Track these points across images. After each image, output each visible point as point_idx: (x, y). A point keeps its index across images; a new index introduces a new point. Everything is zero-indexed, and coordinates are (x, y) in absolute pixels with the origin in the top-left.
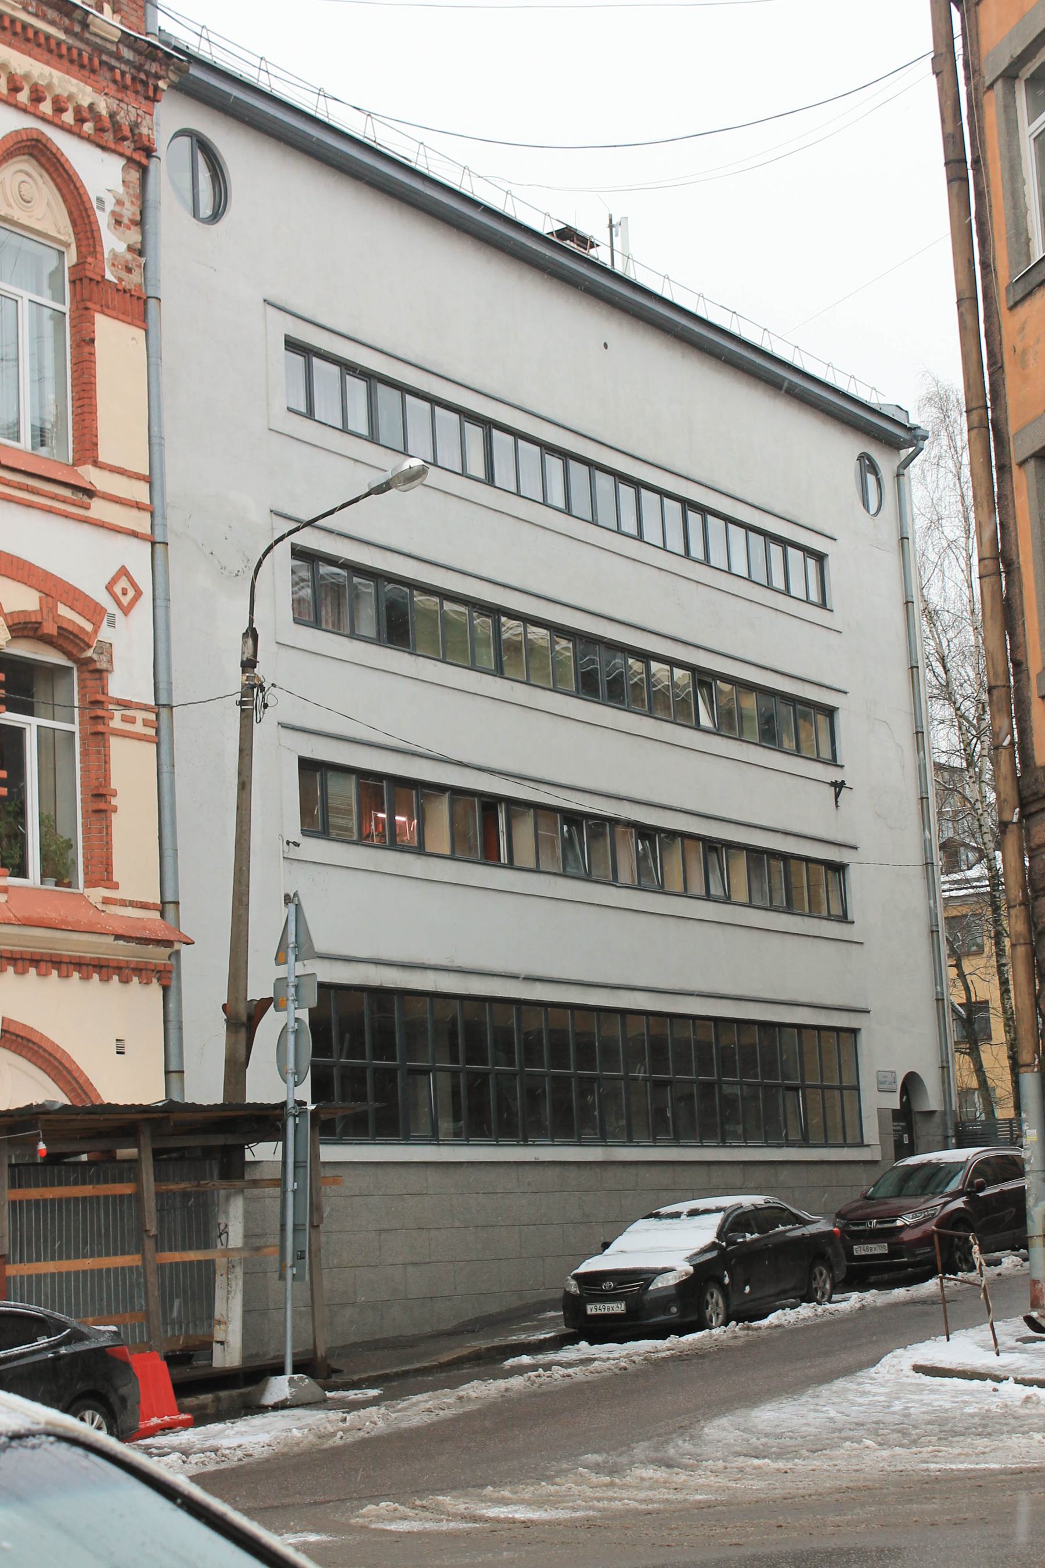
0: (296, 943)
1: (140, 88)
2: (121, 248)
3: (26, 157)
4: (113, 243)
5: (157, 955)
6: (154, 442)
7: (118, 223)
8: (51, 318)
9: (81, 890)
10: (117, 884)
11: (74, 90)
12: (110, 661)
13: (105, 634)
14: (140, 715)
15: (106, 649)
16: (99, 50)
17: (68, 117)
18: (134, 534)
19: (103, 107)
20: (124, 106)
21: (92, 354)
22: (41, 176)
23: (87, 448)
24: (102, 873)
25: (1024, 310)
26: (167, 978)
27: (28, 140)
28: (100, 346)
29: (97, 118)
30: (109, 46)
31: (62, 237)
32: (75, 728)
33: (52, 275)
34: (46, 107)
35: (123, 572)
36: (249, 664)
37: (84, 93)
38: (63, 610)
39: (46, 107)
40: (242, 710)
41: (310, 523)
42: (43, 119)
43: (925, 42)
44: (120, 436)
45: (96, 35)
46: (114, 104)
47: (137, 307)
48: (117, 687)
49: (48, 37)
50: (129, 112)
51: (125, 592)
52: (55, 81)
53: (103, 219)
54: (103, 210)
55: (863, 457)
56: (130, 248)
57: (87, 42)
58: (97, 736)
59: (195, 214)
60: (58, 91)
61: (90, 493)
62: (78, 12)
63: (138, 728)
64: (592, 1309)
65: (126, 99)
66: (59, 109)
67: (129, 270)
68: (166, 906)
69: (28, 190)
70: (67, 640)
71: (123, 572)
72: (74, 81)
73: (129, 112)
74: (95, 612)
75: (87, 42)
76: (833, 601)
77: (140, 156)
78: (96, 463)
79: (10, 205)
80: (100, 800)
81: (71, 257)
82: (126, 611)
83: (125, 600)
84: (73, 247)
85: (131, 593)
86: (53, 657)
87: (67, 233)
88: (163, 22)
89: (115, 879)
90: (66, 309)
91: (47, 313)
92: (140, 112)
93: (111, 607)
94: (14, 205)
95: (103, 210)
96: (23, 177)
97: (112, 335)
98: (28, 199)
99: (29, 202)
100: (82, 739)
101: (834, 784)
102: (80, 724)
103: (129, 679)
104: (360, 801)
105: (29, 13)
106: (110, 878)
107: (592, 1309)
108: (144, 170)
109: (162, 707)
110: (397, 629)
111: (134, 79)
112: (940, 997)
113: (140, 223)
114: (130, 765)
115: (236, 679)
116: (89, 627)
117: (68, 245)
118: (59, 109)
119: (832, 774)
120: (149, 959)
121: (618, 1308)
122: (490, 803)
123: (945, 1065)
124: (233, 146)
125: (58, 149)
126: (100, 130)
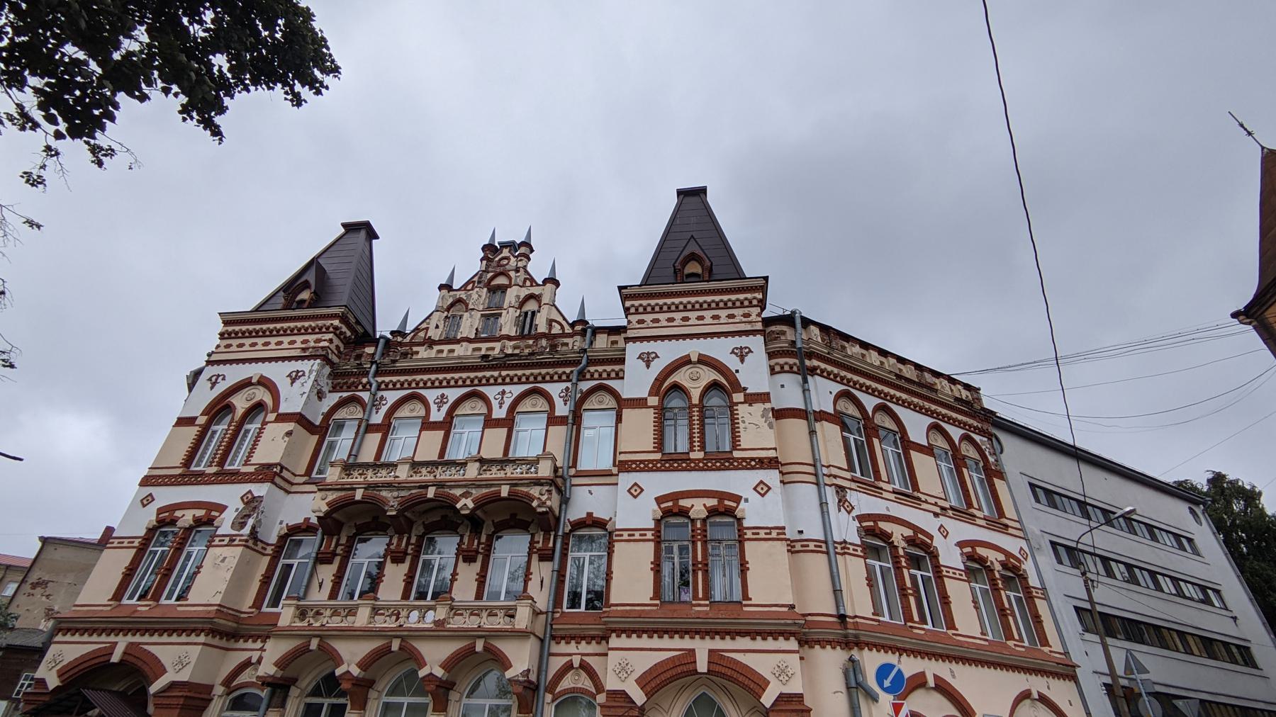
26: (1073, 678)
68: (1066, 653)
81: (981, 464)
109: (1044, 589)
124: (1002, 436)
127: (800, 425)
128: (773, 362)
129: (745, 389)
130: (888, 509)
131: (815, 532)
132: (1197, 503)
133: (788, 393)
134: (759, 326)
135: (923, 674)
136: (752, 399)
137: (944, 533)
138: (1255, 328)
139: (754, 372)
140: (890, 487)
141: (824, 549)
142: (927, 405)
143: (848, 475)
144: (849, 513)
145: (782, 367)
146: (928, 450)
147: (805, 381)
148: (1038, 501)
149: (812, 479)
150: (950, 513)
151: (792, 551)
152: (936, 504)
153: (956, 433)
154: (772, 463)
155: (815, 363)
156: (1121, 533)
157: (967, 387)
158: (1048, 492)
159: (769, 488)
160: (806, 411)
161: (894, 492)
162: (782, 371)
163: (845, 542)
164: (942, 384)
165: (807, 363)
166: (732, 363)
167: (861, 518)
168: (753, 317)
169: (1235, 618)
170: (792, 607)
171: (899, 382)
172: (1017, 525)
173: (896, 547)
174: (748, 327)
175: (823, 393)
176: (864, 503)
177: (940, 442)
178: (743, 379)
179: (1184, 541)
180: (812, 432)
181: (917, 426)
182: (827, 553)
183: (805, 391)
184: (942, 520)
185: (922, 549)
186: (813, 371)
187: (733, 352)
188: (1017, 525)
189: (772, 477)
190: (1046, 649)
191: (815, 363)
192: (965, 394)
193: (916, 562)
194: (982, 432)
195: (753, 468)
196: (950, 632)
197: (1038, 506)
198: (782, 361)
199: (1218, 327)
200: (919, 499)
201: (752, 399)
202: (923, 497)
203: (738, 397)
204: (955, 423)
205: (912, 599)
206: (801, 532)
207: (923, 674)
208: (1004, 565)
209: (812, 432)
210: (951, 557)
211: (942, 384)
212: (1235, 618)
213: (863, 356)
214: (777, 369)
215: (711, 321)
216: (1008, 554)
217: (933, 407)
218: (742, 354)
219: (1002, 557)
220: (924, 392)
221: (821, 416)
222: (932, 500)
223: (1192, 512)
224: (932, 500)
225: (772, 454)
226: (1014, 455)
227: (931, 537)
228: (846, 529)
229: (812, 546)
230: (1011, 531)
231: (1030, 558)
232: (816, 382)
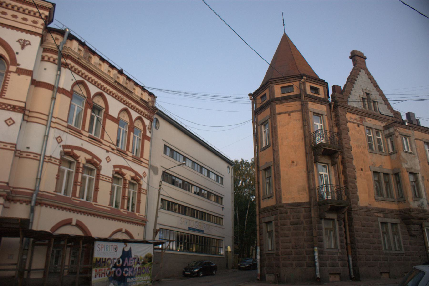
5: (144, 223)
6: (150, 156)
14: (145, 191)
15: (101, 166)
16: (149, 108)
17: (144, 115)
19: (148, 114)
23: (142, 156)
24: (138, 211)
25: (262, 152)
26: (145, 225)
34: (142, 114)
35: (145, 172)
36: (160, 186)
37: (146, 112)
39: (142, 114)
41: (168, 169)
42: (102, 90)
43: (251, 118)
44: (146, 155)
48: (143, 187)
50: (151, 115)
53: (147, 128)
55: (228, 166)
58: (140, 193)
61: (142, 162)
63: (144, 192)
64: (186, 273)
66: (144, 114)
68: (146, 216)
70: (95, 164)
71: (145, 172)
73: (151, 115)
74: (141, 177)
76: (224, 183)
77: (151, 121)
78: (143, 158)
80: (139, 202)
81: (142, 132)
82: (145, 177)
88: (156, 105)
90: (141, 138)
97: (146, 142)
104: (170, 205)
107: (186, 273)
108: (152, 122)
109: (148, 190)
110: (173, 183)
113: (151, 129)
114: (143, 197)
115: (158, 187)
118: (144, 114)
119: (222, 206)
120: (143, 223)
121: (189, 273)
122: (186, 207)
124: (161, 121)
127: (47, 93)
128: (45, 54)
129: (18, 65)
130: (82, 145)
131: (36, 148)
132: (231, 165)
133: (48, 73)
134: (40, 31)
135: (71, 219)
136: (21, 71)
137: (108, 159)
138: (252, 102)
139: (28, 58)
140: (87, 134)
141: (38, 158)
142: (125, 98)
143: (66, 124)
144: (59, 143)
145: (49, 59)
146: (117, 121)
147: (59, 70)
148: (165, 153)
149: (45, 122)
150: (115, 152)
151: (15, 156)
152: (110, 147)
153: (135, 115)
154: (22, 110)
155: (68, 61)
156: (196, 172)
157: (151, 94)
158: (172, 150)
159: (6, 121)
160: (54, 86)
161: (89, 137)
162: (49, 60)
163: (51, 157)
164: (138, 92)
165: (63, 60)
166: (16, 47)
167: (65, 147)
168: (39, 25)
169: (223, 208)
170: (8, 184)
171: (116, 86)
172: (147, 162)
173: (79, 163)
174: (33, 30)
175: (67, 79)
176: (71, 140)
177: (125, 118)
178: (19, 59)
179: (220, 178)
180: (54, 98)
181: (115, 107)
182: (39, 160)
183: (58, 76)
184: (110, 154)
185: (94, 164)
186: (66, 65)
187: (18, 41)
188: (147, 162)
189: (18, 117)
190: (137, 214)
191: (68, 61)
192: (146, 97)
193: (90, 171)
194: (148, 118)
195: (8, 110)
196: (94, 203)
197: (165, 155)
198: (50, 55)
199: (243, 98)
200: (102, 143)
201: (21, 71)
202: (104, 142)
203: (13, 68)
204: (136, 110)
205: (78, 188)
206: (28, 148)
207: (71, 219)
208: (133, 178)
209: (54, 98)
210: (107, 170)
211: (138, 92)
212: (223, 208)
213: (100, 65)
214: (46, 58)
215: (11, 18)
216: (136, 173)
217: (128, 100)
218: (24, 44)
219: (133, 174)
220: (126, 92)
221: (63, 91)
222: (108, 144)
223: (228, 167)
224: (108, 144)
225: (23, 105)
226: (165, 131)
227: (100, 161)
228: (54, 150)
229: (32, 156)
230: (143, 164)
231: (147, 177)
232: (65, 72)
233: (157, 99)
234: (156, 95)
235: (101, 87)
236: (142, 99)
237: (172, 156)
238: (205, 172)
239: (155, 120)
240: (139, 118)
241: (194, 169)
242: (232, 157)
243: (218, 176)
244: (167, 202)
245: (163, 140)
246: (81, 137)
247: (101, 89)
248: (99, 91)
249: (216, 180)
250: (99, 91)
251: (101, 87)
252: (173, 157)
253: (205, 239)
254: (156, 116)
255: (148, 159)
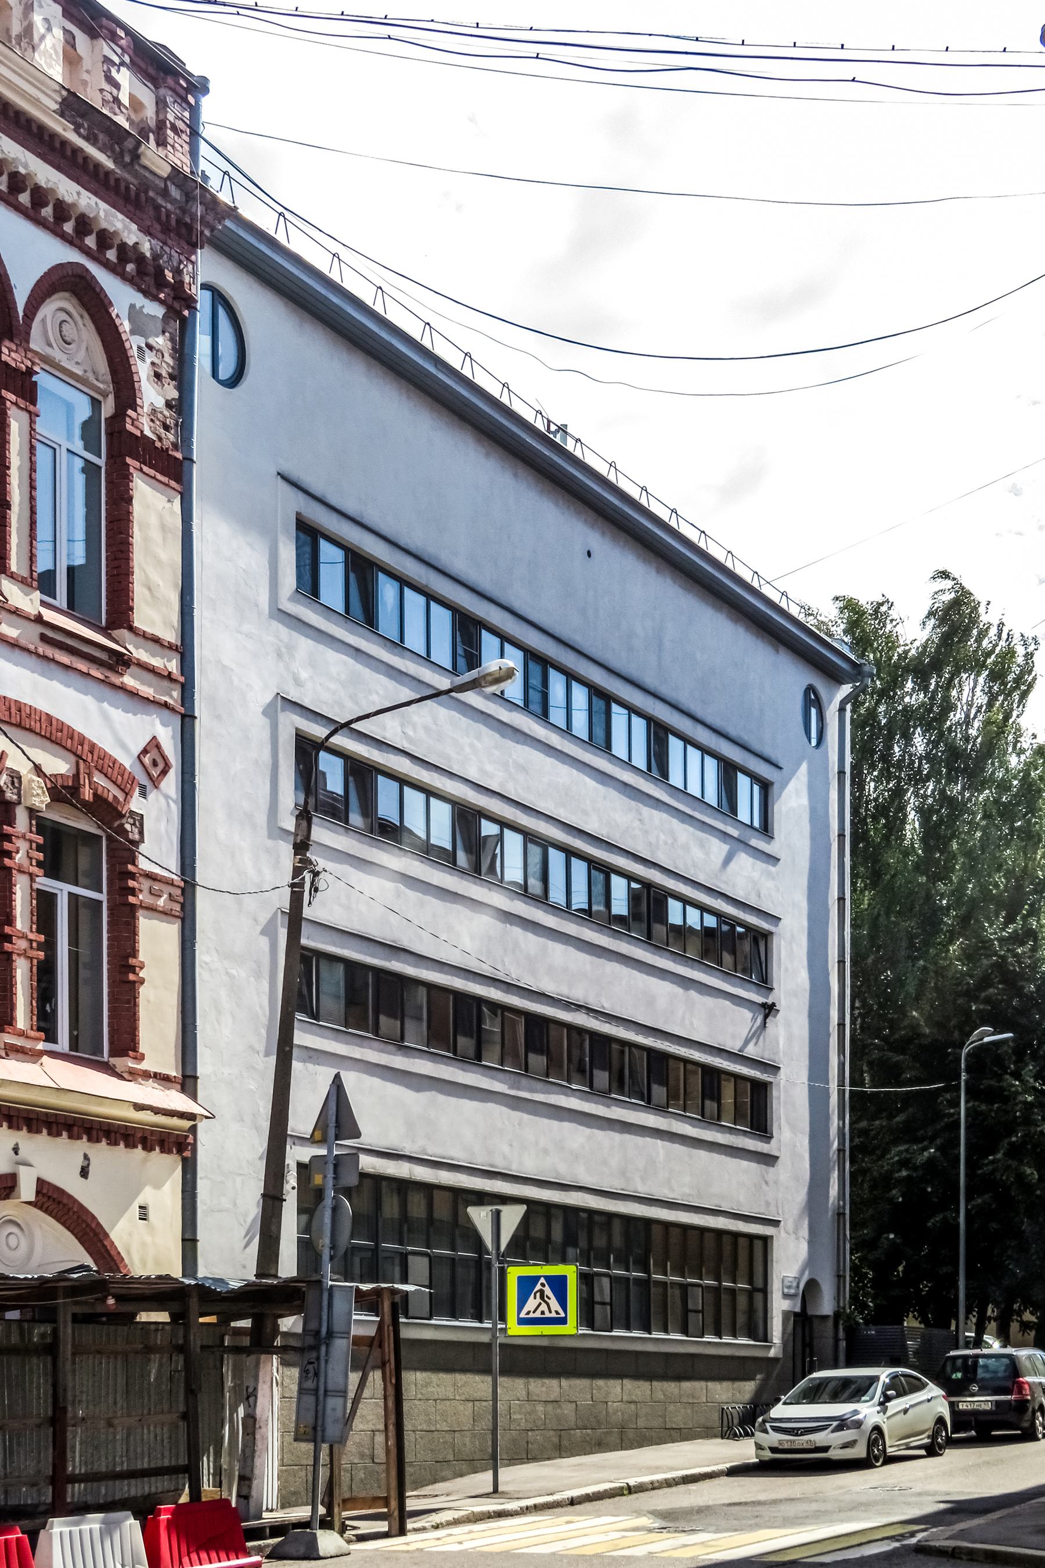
0: (338, 1119)
1: (184, 231)
2: (160, 403)
3: (66, 294)
4: (152, 396)
7: (158, 376)
8: (83, 470)
9: (106, 1059)
10: (143, 1055)
11: (119, 226)
12: (141, 833)
13: (136, 804)
15: (139, 820)
17: (111, 255)
18: (166, 705)
19: (146, 247)
20: (167, 249)
21: (129, 513)
22: (82, 317)
23: (120, 615)
27: (73, 275)
28: (137, 509)
29: (140, 259)
30: (157, 181)
31: (101, 386)
32: (103, 897)
33: (85, 425)
34: (90, 241)
37: (129, 232)
38: (98, 779)
39: (90, 241)
40: (293, 892)
42: (86, 252)
45: (145, 168)
46: (157, 245)
47: (174, 469)
49: (98, 165)
51: (155, 764)
52: (102, 214)
54: (143, 360)
55: (810, 689)
56: (168, 405)
57: (136, 175)
59: (215, 374)
60: (104, 225)
62: (130, 140)
65: (170, 242)
67: (166, 428)
69: (69, 330)
72: (120, 216)
74: (126, 784)
75: (136, 175)
77: (179, 305)
78: (131, 629)
79: (50, 345)
81: (108, 408)
83: (155, 773)
84: (111, 398)
85: (161, 766)
86: (86, 825)
87: (104, 382)
89: (141, 1050)
90: (101, 462)
91: (79, 463)
92: (182, 258)
93: (143, 779)
94: (54, 345)
95: (143, 360)
96: (63, 316)
97: (150, 502)
98: (68, 339)
99: (69, 344)
100: (109, 909)
101: (764, 1005)
102: (108, 893)
103: (157, 852)
105: (80, 135)
106: (135, 1049)
111: (178, 221)
112: (841, 1211)
116: (121, 797)
117: (105, 396)
123: (841, 1273)
125: (102, 288)
126: (141, 272)
157: (156, 66)
194: (148, 277)
202: (141, 653)
233: (209, 107)
234: (195, 67)
235: (80, 230)
236: (73, 106)
237: (364, 611)
238: (629, 736)
239: (203, 300)
240: (61, 281)
241: (544, 715)
242: (809, 589)
243: (729, 770)
244: (341, 968)
245: (279, 474)
246: (44, 638)
247: (74, 241)
248: (73, 256)
249: (711, 797)
250: (73, 256)
251: (80, 230)
252: (369, 619)
253: (735, 1245)
254: (207, 268)
255: (171, 636)
